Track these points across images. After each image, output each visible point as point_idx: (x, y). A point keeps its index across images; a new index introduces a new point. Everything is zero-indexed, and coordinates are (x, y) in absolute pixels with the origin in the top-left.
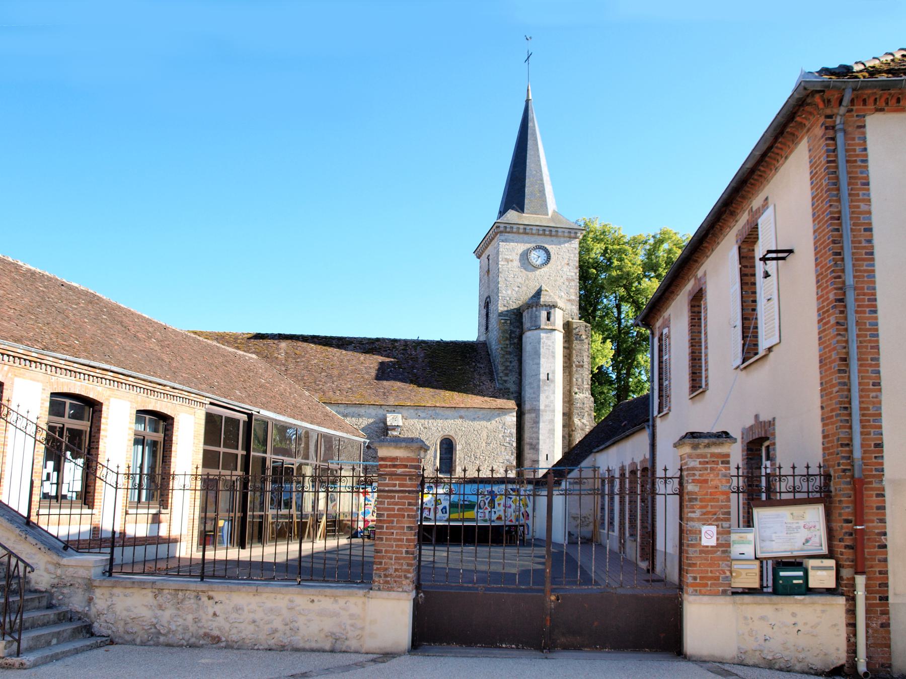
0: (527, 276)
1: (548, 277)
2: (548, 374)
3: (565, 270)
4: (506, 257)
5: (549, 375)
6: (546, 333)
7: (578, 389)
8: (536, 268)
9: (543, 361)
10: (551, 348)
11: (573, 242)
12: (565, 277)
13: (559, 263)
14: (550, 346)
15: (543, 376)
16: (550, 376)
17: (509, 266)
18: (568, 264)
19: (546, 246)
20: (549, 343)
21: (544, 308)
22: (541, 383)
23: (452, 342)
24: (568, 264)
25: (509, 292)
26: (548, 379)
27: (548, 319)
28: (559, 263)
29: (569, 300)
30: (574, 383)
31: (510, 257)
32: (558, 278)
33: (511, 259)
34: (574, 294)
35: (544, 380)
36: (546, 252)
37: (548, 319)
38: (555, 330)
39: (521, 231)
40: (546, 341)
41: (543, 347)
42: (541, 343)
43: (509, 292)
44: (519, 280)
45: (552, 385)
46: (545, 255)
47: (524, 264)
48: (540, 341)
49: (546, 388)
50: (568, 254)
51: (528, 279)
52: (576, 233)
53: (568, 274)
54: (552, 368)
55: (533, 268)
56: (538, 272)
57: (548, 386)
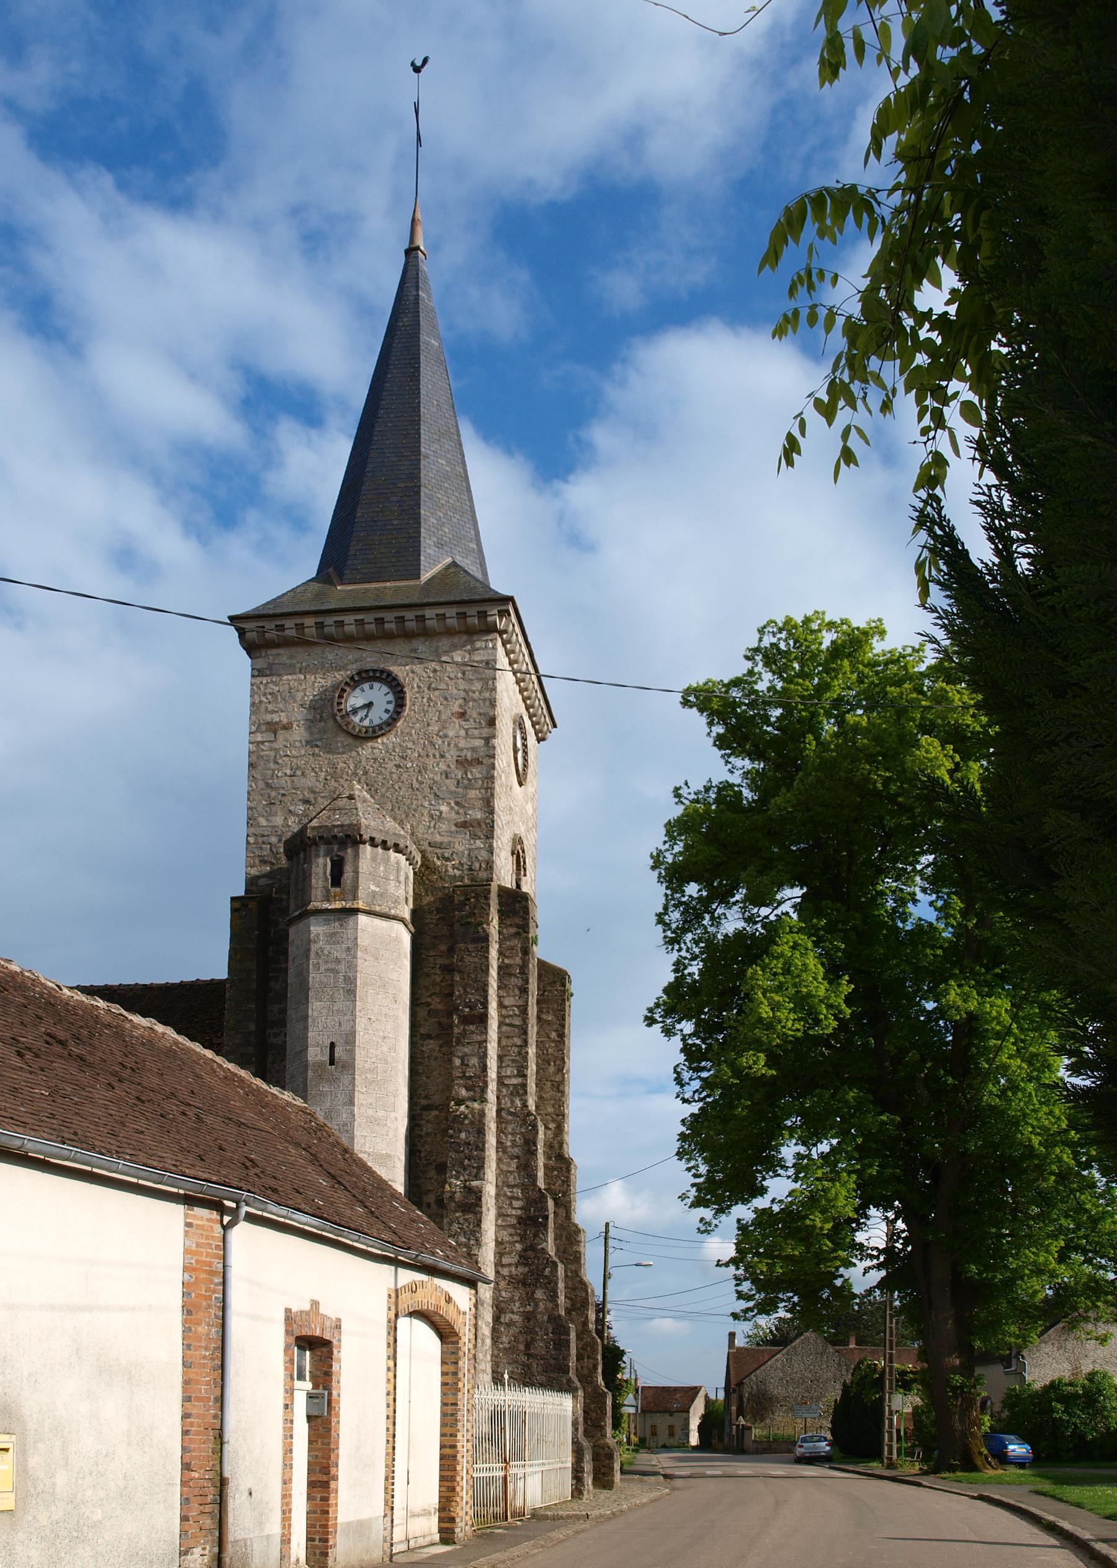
0: (334, 766)
1: (398, 761)
2: (332, 1046)
3: (451, 733)
4: (268, 718)
5: (337, 1049)
6: (327, 922)
7: (468, 1089)
8: (372, 734)
9: (316, 1007)
10: (342, 967)
11: (478, 644)
12: (452, 755)
13: (433, 716)
14: (338, 961)
15: (316, 1054)
16: (339, 1052)
17: (279, 744)
18: (462, 715)
19: (395, 669)
20: (338, 952)
21: (322, 849)
22: (310, 1073)
23: (182, 985)
24: (462, 715)
25: (279, 820)
26: (332, 1062)
27: (337, 878)
28: (433, 716)
29: (464, 825)
30: (457, 1073)
31: (283, 718)
32: (430, 762)
33: (285, 721)
34: (479, 804)
35: (320, 1065)
36: (391, 687)
37: (337, 878)
38: (355, 911)
39: (311, 632)
40: (328, 947)
41: (317, 966)
42: (312, 955)
43: (279, 820)
44: (310, 781)
45: (345, 1079)
46: (391, 697)
47: (323, 731)
48: (309, 950)
49: (326, 1088)
50: (463, 685)
51: (335, 776)
52: (483, 615)
53: (462, 744)
54: (346, 1027)
55: (350, 740)
56: (366, 751)
57: (333, 1080)
